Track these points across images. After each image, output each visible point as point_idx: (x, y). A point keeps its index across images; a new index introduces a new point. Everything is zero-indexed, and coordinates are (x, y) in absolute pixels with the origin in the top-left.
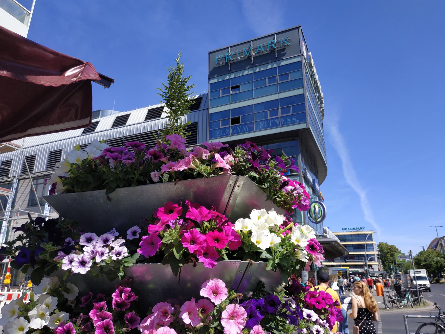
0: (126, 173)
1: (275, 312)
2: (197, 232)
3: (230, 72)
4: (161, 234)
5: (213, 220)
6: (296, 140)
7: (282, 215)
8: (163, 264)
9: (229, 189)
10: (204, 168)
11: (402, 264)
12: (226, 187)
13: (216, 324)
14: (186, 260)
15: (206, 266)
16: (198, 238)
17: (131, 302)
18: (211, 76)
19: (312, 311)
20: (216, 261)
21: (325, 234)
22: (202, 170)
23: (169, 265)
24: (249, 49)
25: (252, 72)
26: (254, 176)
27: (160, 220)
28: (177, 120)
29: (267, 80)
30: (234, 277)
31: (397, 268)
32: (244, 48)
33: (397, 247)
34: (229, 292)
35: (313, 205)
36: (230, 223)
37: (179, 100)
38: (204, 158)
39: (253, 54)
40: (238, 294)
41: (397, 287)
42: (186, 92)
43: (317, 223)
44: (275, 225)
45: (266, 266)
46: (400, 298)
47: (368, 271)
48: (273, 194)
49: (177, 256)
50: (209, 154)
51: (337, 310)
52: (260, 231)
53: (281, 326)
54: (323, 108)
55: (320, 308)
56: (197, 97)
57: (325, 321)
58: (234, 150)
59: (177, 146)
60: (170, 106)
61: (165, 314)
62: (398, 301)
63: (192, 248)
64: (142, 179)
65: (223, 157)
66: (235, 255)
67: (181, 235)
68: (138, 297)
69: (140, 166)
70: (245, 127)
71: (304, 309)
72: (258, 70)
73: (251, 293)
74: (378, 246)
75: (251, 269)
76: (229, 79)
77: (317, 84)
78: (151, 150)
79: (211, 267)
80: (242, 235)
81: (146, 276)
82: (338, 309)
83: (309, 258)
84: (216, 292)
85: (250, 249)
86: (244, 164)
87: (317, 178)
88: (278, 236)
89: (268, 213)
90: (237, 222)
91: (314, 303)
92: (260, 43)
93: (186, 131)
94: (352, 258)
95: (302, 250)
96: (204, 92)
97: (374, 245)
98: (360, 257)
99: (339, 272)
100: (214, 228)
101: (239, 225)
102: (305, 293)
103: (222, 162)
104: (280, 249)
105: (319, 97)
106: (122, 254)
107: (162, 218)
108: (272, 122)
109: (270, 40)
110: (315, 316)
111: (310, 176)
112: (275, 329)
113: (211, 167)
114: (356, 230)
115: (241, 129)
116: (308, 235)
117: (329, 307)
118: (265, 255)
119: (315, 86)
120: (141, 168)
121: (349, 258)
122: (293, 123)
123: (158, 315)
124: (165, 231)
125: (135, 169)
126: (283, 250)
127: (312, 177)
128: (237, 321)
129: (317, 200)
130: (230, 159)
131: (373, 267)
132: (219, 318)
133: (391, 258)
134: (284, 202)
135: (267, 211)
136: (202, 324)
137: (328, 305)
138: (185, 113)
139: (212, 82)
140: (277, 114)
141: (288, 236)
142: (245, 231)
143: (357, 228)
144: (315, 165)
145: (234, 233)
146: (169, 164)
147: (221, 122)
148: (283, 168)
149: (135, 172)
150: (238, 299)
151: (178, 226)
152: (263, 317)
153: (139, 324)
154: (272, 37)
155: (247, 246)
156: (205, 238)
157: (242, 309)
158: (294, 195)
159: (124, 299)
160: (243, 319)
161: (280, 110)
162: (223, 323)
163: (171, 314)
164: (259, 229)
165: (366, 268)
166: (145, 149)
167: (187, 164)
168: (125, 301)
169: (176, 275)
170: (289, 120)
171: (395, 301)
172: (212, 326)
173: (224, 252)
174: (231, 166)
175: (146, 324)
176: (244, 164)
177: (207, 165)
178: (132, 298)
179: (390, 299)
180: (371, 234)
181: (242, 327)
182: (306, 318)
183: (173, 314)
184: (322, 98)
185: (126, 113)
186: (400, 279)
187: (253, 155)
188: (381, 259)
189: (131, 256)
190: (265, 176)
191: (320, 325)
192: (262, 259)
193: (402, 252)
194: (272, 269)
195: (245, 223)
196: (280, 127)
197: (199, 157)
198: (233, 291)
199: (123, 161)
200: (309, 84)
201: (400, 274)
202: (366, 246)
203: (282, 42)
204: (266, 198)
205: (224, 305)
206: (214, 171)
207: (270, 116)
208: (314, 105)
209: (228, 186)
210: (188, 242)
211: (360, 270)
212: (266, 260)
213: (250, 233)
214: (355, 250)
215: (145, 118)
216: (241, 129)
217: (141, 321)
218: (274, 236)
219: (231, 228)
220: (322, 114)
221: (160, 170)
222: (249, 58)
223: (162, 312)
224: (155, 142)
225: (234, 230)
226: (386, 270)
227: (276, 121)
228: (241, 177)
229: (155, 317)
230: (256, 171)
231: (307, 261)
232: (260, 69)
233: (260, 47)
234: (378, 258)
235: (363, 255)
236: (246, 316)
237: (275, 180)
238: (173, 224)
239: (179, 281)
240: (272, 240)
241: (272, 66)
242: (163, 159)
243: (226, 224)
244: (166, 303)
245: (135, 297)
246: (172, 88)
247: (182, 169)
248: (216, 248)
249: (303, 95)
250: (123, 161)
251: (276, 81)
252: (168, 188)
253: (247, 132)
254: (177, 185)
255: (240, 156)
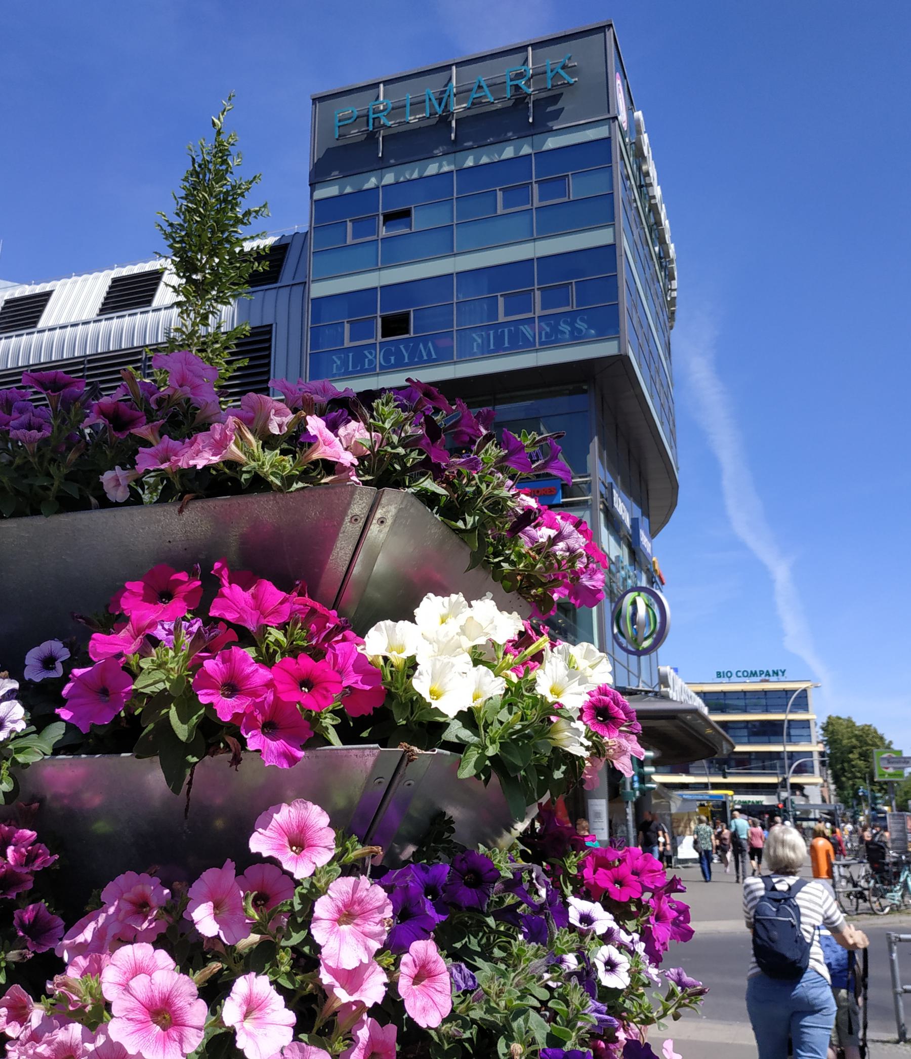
0: (24, 470)
1: (481, 903)
2: (245, 658)
3: (382, 165)
4: (133, 662)
5: (296, 624)
6: (585, 391)
7: (515, 614)
8: (138, 757)
9: (350, 529)
10: (270, 462)
11: (892, 783)
12: (340, 523)
13: (297, 938)
14: (209, 746)
15: (270, 762)
16: (248, 677)
17: (36, 874)
18: (317, 178)
19: (598, 905)
20: (303, 748)
21: (663, 689)
22: (267, 468)
23: (157, 759)
24: (444, 92)
25: (452, 168)
26: (434, 493)
27: (127, 620)
28: (205, 318)
29: (500, 194)
30: (357, 800)
31: (879, 795)
32: (429, 89)
33: (880, 731)
34: (340, 841)
35: (630, 597)
36: (350, 634)
37: (212, 254)
38: (275, 431)
39: (457, 108)
40: (367, 849)
41: (874, 852)
42: (240, 229)
43: (639, 653)
44: (494, 644)
45: (459, 764)
46: (882, 882)
47: (789, 804)
48: (491, 549)
49: (182, 731)
50: (291, 417)
51: (675, 906)
52: (442, 658)
53: (500, 948)
54: (674, 294)
55: (625, 899)
56: (270, 241)
57: (636, 936)
58: (371, 409)
59: (187, 389)
60: (186, 267)
61: (141, 907)
62: (875, 891)
63: (227, 707)
64: (73, 490)
65: (333, 427)
66: (365, 734)
67: (195, 666)
68: (57, 857)
69: (69, 449)
70: (425, 346)
71: (572, 899)
72: (470, 163)
73: (411, 849)
74: (823, 729)
75: (409, 771)
76: (378, 187)
77: (657, 214)
78: (105, 400)
79: (286, 766)
80: (387, 671)
81: (86, 796)
82: (678, 903)
83: (590, 744)
84: (299, 841)
85: (412, 713)
86: (401, 451)
87: (646, 513)
88: (496, 676)
89: (470, 606)
90: (372, 632)
91: (608, 885)
92: (481, 75)
93: (232, 354)
94: (744, 762)
95: (571, 719)
96: (296, 228)
97: (812, 725)
98: (768, 761)
99: (702, 805)
100: (299, 647)
101: (378, 642)
102: (582, 854)
103: (329, 444)
104: (504, 715)
105: (663, 257)
106: (7, 724)
107: (134, 615)
108: (510, 331)
109: (511, 65)
110: (604, 921)
111: (622, 508)
112: (481, 955)
113: (294, 458)
114: (759, 679)
115: (414, 352)
116: (589, 672)
117: (652, 897)
118: (456, 732)
119: (652, 220)
120: (72, 456)
121: (733, 763)
122: (577, 338)
123: (118, 910)
124: (143, 653)
125: (53, 460)
126: (511, 718)
127: (630, 510)
128: (360, 929)
129: (644, 583)
130: (357, 436)
131: (808, 790)
132: (306, 919)
133: (861, 763)
134: (528, 577)
135: (469, 599)
136: (255, 938)
137: (649, 890)
138: (234, 296)
139: (320, 194)
140: (529, 308)
141: (530, 677)
142: (398, 658)
143: (762, 672)
144: (640, 473)
145: (364, 666)
146: (160, 447)
147: (347, 327)
148: (522, 469)
149: (53, 470)
150: (369, 863)
151: (186, 640)
152: (443, 918)
153: (61, 940)
154: (519, 57)
155: (402, 706)
156: (271, 676)
157: (380, 893)
158: (555, 555)
159: (12, 863)
160: (381, 922)
161: (538, 294)
162: (319, 934)
163: (161, 908)
164: (441, 652)
165: (784, 795)
166: (83, 398)
167: (219, 446)
168: (18, 870)
169: (176, 790)
170: (565, 327)
171: (866, 893)
172: (284, 943)
173: (328, 721)
174: (361, 459)
175: (80, 939)
176: (401, 451)
177: (284, 452)
178: (40, 860)
179: (850, 885)
180: (805, 691)
181: (376, 945)
182: (577, 924)
183: (167, 910)
184: (671, 261)
185: (38, 289)
186: (885, 829)
187: (430, 425)
188: (831, 766)
189: (38, 732)
190: (466, 493)
191: (621, 947)
192: (447, 745)
193: (895, 747)
194: (477, 776)
195: (398, 637)
196: (537, 350)
197: (258, 425)
198: (355, 838)
199: (13, 434)
200: (632, 214)
201: (885, 812)
202: (789, 728)
203: (550, 75)
204: (467, 562)
205: (323, 881)
206: (305, 472)
207: (507, 314)
208: (646, 284)
209: (347, 519)
210: (214, 686)
211: (765, 800)
212: (459, 747)
213: (412, 665)
214: (753, 739)
215: (99, 306)
216: (414, 352)
217: (66, 929)
218: (487, 674)
219: (353, 650)
220: (669, 311)
221: (133, 464)
222: (444, 120)
223: (133, 903)
224: (118, 372)
225: (362, 657)
226: (844, 801)
227: (525, 329)
228: (389, 493)
229: (108, 917)
230: (438, 474)
231: (586, 754)
232: (477, 159)
233: (480, 87)
234: (823, 763)
235: (778, 753)
236: (388, 912)
237: (497, 505)
238: (170, 632)
239: (187, 810)
240: (479, 686)
241: (517, 150)
242: (143, 430)
243: (340, 637)
244: (145, 876)
245: (48, 859)
246: (196, 211)
247: (200, 463)
248: (302, 709)
249: (610, 251)
250: (13, 434)
251: (528, 199)
252: (160, 521)
253: (431, 362)
254: (186, 513)
255: (387, 425)
